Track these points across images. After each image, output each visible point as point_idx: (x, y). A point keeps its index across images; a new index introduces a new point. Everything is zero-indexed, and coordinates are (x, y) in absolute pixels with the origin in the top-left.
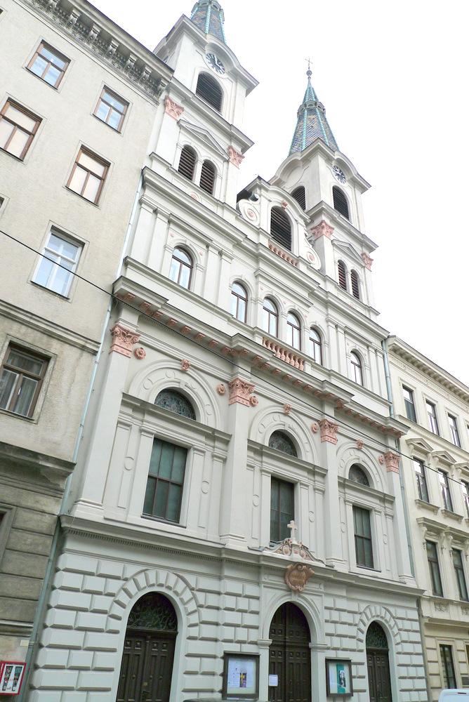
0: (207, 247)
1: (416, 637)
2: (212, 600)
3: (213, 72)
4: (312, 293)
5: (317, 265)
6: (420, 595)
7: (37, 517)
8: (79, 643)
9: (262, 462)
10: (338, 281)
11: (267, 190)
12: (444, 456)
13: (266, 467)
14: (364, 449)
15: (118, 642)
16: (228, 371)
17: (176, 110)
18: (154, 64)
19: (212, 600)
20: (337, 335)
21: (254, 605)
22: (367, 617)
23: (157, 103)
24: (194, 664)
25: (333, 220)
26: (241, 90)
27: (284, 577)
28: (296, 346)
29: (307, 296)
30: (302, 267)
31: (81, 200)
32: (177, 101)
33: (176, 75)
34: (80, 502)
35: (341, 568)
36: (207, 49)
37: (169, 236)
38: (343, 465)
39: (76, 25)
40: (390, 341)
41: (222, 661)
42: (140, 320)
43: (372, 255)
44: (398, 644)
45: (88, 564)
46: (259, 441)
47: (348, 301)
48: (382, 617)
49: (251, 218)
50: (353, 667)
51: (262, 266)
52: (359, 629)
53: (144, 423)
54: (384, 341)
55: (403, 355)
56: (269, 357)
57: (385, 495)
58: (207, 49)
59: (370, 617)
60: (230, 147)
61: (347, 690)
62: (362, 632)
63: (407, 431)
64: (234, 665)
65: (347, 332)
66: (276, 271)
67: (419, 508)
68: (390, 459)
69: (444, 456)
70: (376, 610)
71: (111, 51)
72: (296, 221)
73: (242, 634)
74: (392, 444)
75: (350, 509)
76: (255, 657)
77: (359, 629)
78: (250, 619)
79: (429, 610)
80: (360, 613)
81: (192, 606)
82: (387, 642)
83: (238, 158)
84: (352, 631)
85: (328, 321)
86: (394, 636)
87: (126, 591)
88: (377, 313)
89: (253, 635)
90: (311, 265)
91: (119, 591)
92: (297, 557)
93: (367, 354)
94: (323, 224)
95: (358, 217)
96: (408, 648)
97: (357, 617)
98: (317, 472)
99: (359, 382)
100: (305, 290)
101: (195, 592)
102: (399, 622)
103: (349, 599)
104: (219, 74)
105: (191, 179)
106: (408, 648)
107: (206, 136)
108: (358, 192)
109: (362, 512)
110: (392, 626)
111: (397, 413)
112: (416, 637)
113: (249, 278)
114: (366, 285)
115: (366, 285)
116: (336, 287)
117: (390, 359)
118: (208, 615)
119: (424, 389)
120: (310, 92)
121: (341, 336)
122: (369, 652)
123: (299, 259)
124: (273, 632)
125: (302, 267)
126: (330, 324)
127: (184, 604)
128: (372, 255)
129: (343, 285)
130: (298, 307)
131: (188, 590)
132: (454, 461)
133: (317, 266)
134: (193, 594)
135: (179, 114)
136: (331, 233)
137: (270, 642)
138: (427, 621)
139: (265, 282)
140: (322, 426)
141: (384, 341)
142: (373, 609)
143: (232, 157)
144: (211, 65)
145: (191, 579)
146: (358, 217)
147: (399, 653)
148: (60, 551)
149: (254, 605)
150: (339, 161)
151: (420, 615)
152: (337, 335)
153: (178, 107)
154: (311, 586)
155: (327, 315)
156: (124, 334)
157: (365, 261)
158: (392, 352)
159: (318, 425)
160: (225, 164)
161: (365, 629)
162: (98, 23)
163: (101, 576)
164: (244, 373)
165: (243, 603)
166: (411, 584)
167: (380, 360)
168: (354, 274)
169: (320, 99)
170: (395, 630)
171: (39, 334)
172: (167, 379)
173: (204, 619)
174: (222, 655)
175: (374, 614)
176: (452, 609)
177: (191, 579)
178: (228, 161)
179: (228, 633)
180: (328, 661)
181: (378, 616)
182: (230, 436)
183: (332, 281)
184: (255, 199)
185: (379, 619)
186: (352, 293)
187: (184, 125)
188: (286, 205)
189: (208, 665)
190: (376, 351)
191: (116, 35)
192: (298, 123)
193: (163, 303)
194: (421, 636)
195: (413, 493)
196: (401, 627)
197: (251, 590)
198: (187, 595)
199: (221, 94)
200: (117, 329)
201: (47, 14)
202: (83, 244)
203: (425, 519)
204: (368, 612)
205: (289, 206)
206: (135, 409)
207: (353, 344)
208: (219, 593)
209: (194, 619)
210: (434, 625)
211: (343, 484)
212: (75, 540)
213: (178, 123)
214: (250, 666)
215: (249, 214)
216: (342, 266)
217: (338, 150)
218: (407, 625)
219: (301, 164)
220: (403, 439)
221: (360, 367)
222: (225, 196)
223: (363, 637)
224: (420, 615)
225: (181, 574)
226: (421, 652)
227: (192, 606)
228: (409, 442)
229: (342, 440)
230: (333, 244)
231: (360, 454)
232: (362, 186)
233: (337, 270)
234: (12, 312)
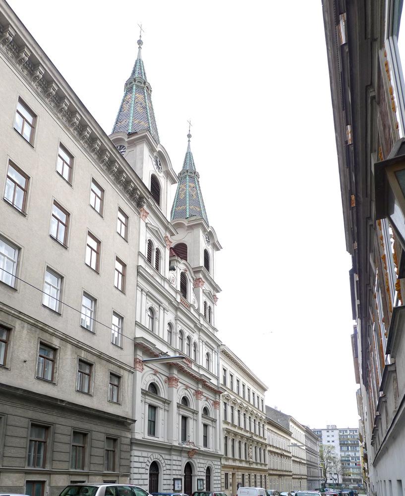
0: (159, 306)
1: (219, 471)
2: (169, 462)
4: (196, 325)
7: (126, 439)
8: (140, 478)
9: (145, 398)
10: (146, 257)
11: (180, 263)
14: (158, 375)
15: (147, 476)
16: (214, 396)
18: (142, 189)
19: (169, 462)
20: (142, 296)
22: (151, 459)
24: (165, 482)
25: (205, 276)
27: (188, 453)
30: (192, 311)
31: (56, 243)
35: (176, 444)
36: (155, 154)
39: (107, 162)
40: (222, 347)
41: (173, 481)
43: (218, 295)
45: (139, 453)
47: (206, 325)
48: (158, 459)
51: (179, 314)
52: (147, 465)
54: (219, 346)
55: (226, 354)
57: (195, 411)
58: (155, 154)
59: (152, 458)
61: (202, 488)
62: (148, 466)
64: (176, 482)
65: (148, 295)
66: (159, 294)
67: (224, 423)
68: (199, 394)
70: (155, 456)
71: (96, 148)
74: (218, 396)
75: (147, 406)
76: (181, 479)
77: (147, 465)
79: (224, 462)
82: (158, 470)
84: (144, 465)
85: (199, 339)
88: (217, 331)
89: (180, 473)
90: (172, 284)
92: (192, 447)
96: (217, 474)
98: (167, 402)
100: (192, 323)
102: (166, 461)
103: (203, 459)
106: (217, 474)
109: (153, 408)
112: (219, 471)
113: (173, 322)
117: (220, 356)
118: (168, 467)
119: (231, 369)
120: (139, 65)
121: (144, 297)
122: (151, 474)
123: (191, 305)
124: (185, 471)
125: (192, 311)
128: (218, 295)
129: (149, 259)
132: (231, 398)
136: (146, 217)
137: (185, 474)
139: (181, 324)
140: (198, 393)
141: (219, 346)
145: (163, 456)
148: (131, 450)
150: (160, 152)
151: (221, 464)
152: (142, 296)
154: (195, 456)
155: (200, 335)
157: (214, 299)
161: (150, 465)
162: (118, 162)
164: (175, 372)
166: (220, 453)
168: (158, 252)
169: (150, 79)
171: (117, 367)
176: (237, 462)
178: (165, 247)
179: (174, 472)
180: (198, 479)
182: (171, 401)
185: (157, 460)
186: (154, 266)
189: (169, 482)
191: (127, 170)
192: (126, 96)
195: (222, 418)
197: (179, 458)
201: (32, 83)
202: (19, 249)
203: (227, 428)
204: (152, 457)
205: (188, 272)
207: (151, 303)
209: (165, 468)
210: (225, 467)
211: (179, 407)
212: (135, 446)
214: (180, 482)
216: (150, 244)
217: (159, 143)
218: (217, 467)
219: (186, 228)
221: (153, 319)
223: (148, 468)
224: (221, 464)
228: (223, 396)
230: (147, 226)
231: (206, 402)
232: (217, 247)
234: (110, 360)
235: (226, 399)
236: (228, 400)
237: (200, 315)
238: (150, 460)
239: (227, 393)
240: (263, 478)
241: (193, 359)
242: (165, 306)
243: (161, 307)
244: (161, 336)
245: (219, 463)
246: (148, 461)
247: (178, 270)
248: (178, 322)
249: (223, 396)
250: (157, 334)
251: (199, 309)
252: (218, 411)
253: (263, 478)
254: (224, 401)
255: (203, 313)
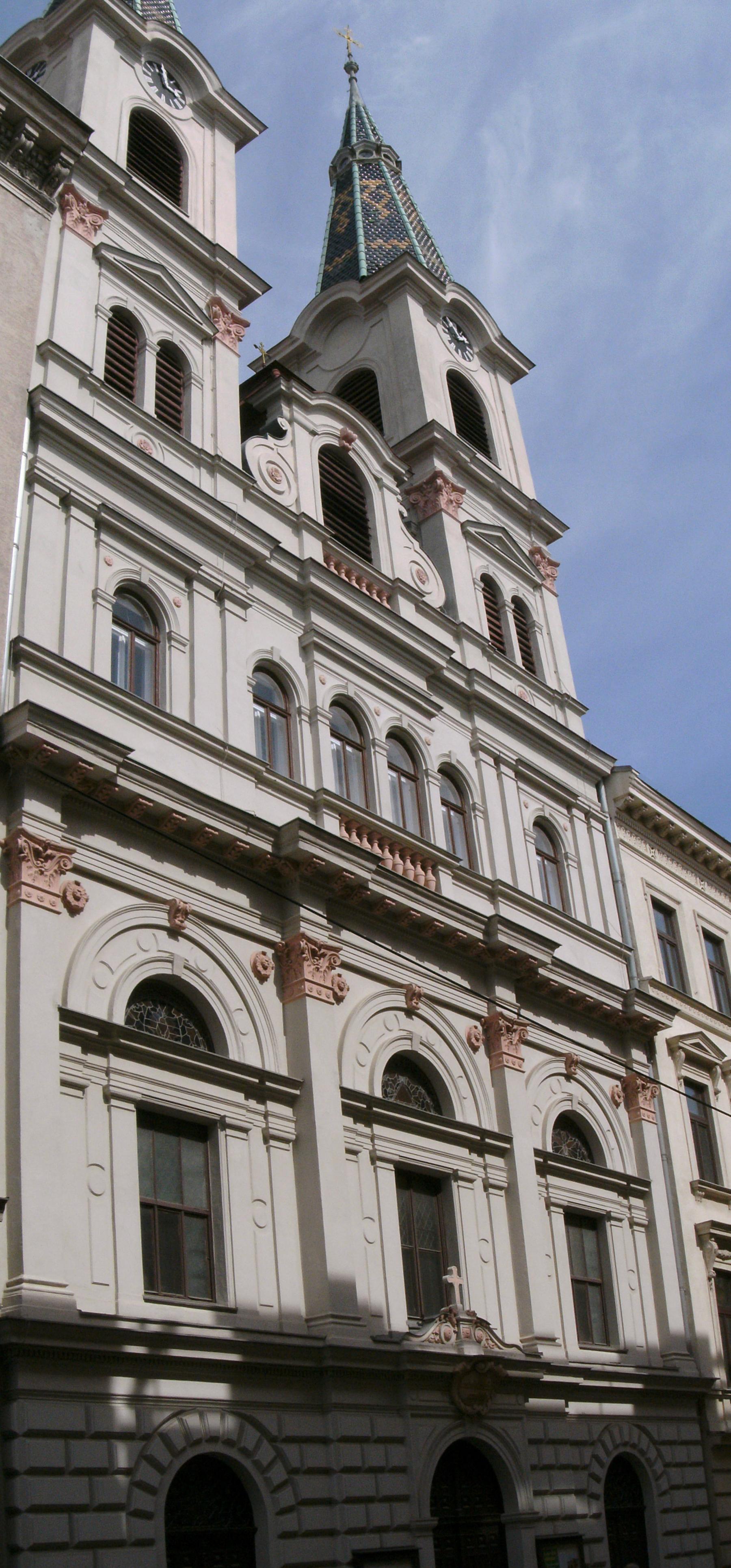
1: (696, 1475)
2: (316, 1456)
3: (161, 107)
5: (436, 598)
6: (704, 1390)
10: (487, 634)
12: (697, 1045)
13: (385, 1149)
14: (580, 1075)
17: (89, 218)
19: (316, 1456)
21: (397, 1455)
23: (50, 208)
25: (460, 468)
26: (225, 146)
28: (413, 827)
29: (425, 688)
30: (407, 609)
32: (91, 196)
33: (93, 139)
34: (24, 1285)
37: (102, 564)
38: (540, 1119)
42: (67, 815)
43: (551, 551)
44: (664, 1493)
46: (364, 1089)
47: (511, 684)
48: (634, 1446)
49: (277, 487)
50: (586, 1549)
53: (112, 1076)
56: (369, 870)
59: (610, 1446)
60: (217, 301)
62: (598, 1480)
63: (671, 1019)
69: (697, 1045)
72: (377, 479)
73: (380, 1514)
74: (638, 1055)
78: (391, 1484)
80: (593, 1444)
81: (278, 1474)
83: (233, 328)
85: (476, 748)
86: (657, 1479)
87: (152, 1461)
89: (403, 1514)
91: (137, 1463)
93: (568, 825)
94: (439, 481)
95: (512, 449)
96: (682, 1498)
97: (588, 1452)
99: (556, 903)
101: (279, 1445)
104: (174, 111)
105: (131, 397)
106: (682, 1498)
107: (158, 278)
108: (504, 383)
110: (645, 1448)
111: (646, 974)
112: (696, 1475)
114: (549, 634)
115: (549, 634)
116: (484, 652)
117: (621, 834)
121: (510, 784)
123: (396, 587)
125: (407, 609)
126: (482, 755)
127: (264, 1470)
128: (551, 551)
130: (410, 719)
131: (265, 1443)
133: (436, 598)
134: (276, 1449)
135: (96, 228)
136: (459, 505)
137: (435, 1522)
138: (718, 1441)
142: (616, 1431)
143: (221, 326)
144: (155, 89)
145: (268, 1420)
146: (512, 449)
147: (665, 1511)
149: (397, 1455)
150: (455, 305)
153: (92, 209)
155: (474, 731)
156: (37, 854)
158: (625, 816)
159: (480, 1028)
160: (207, 349)
161: (602, 1473)
163: (79, 1472)
165: (375, 1455)
167: (599, 838)
168: (519, 605)
170: (659, 1467)
172: (142, 957)
173: (307, 1494)
174: (349, 1557)
175: (618, 1441)
177: (268, 1420)
179: (355, 1515)
181: (625, 1444)
183: (474, 637)
184: (279, 433)
185: (628, 1450)
186: (519, 661)
187: (110, 256)
188: (350, 440)
190: (588, 815)
193: (120, 759)
194: (706, 1472)
196: (668, 1459)
197: (387, 1425)
198: (266, 1453)
199: (180, 159)
200: (21, 841)
203: (715, 1224)
204: (607, 1438)
206: (89, 1045)
208: (324, 1441)
209: (286, 1498)
213: (96, 250)
215: (272, 476)
216: (489, 585)
218: (680, 1454)
220: (661, 1039)
222: (214, 435)
224: (705, 1431)
225: (248, 1412)
226: (705, 1503)
227: (278, 1474)
228: (672, 1047)
229: (533, 1058)
231: (573, 1088)
233: (480, 595)
235: (693, 1060)
236: (707, 1067)
237: (460, 631)
238: (601, 1453)
239: (693, 1029)
240: (548, 1455)
241: (388, 816)
242: (220, 580)
243: (575, 812)
244: (597, 925)
245: (692, 1432)
246: (595, 1457)
247: (302, 435)
248: (318, 656)
249: (672, 1047)
250: (582, 918)
251: (450, 604)
252: (650, 1132)
253: (548, 1455)
254: (684, 1073)
255: (482, 627)
